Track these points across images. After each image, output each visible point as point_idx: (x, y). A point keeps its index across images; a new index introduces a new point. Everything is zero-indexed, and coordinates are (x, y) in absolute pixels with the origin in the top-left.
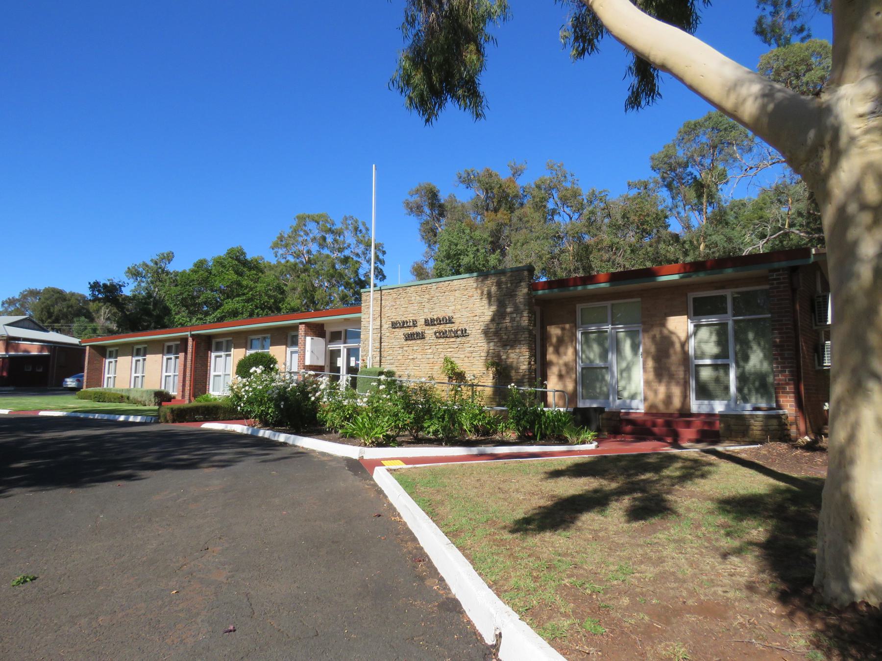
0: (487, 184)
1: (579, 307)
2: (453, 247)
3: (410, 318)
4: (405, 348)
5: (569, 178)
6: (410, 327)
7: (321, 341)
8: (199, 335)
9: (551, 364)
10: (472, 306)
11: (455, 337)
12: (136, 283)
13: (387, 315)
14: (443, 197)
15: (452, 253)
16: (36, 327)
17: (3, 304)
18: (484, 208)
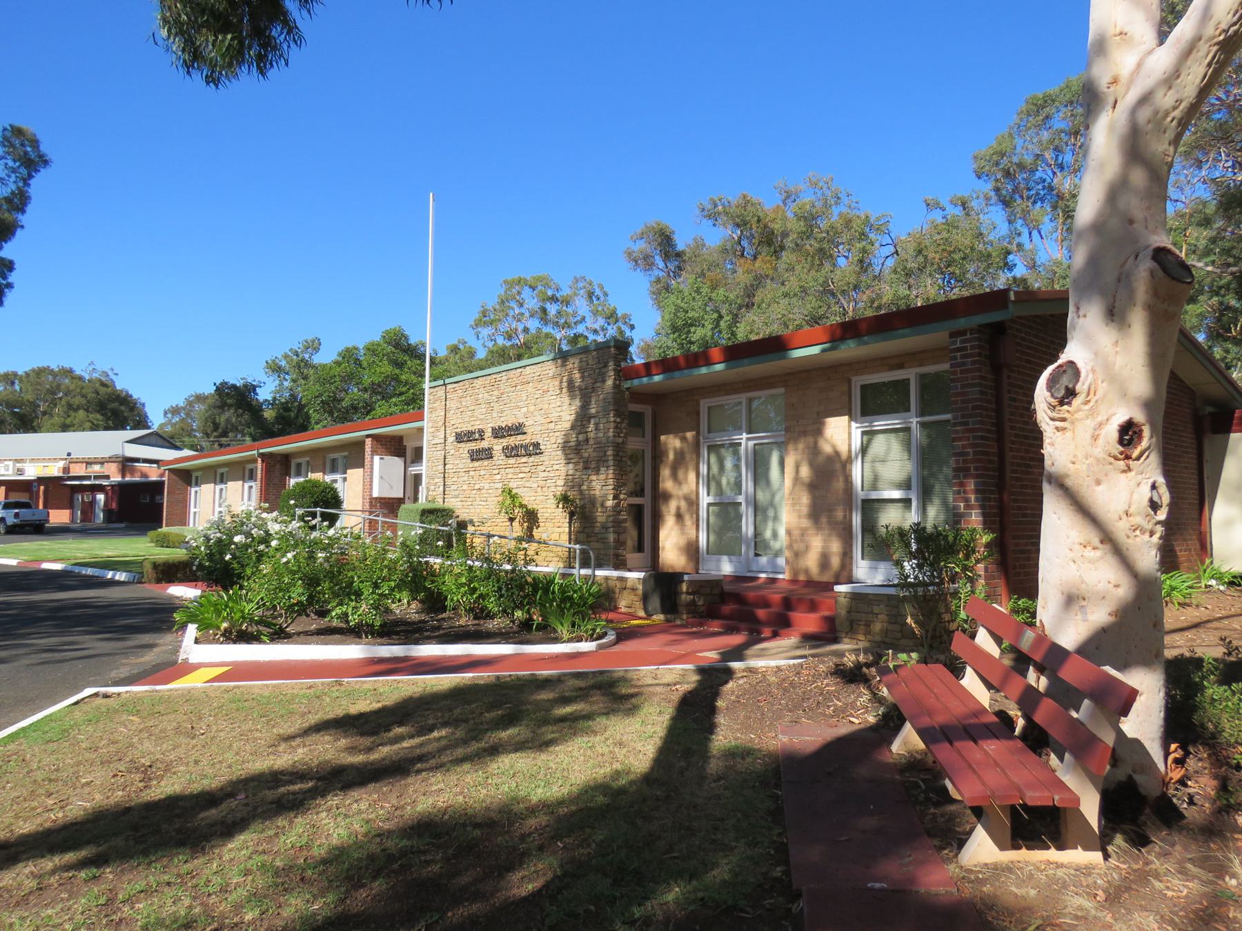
0: (738, 216)
1: (704, 404)
2: (681, 314)
3: (477, 426)
4: (472, 473)
5: (845, 200)
6: (476, 440)
7: (397, 462)
8: (271, 455)
9: (667, 497)
10: (546, 406)
11: (527, 455)
12: (277, 382)
13: (452, 422)
14: (682, 242)
15: (680, 323)
16: (166, 444)
17: (166, 413)
18: (735, 251)
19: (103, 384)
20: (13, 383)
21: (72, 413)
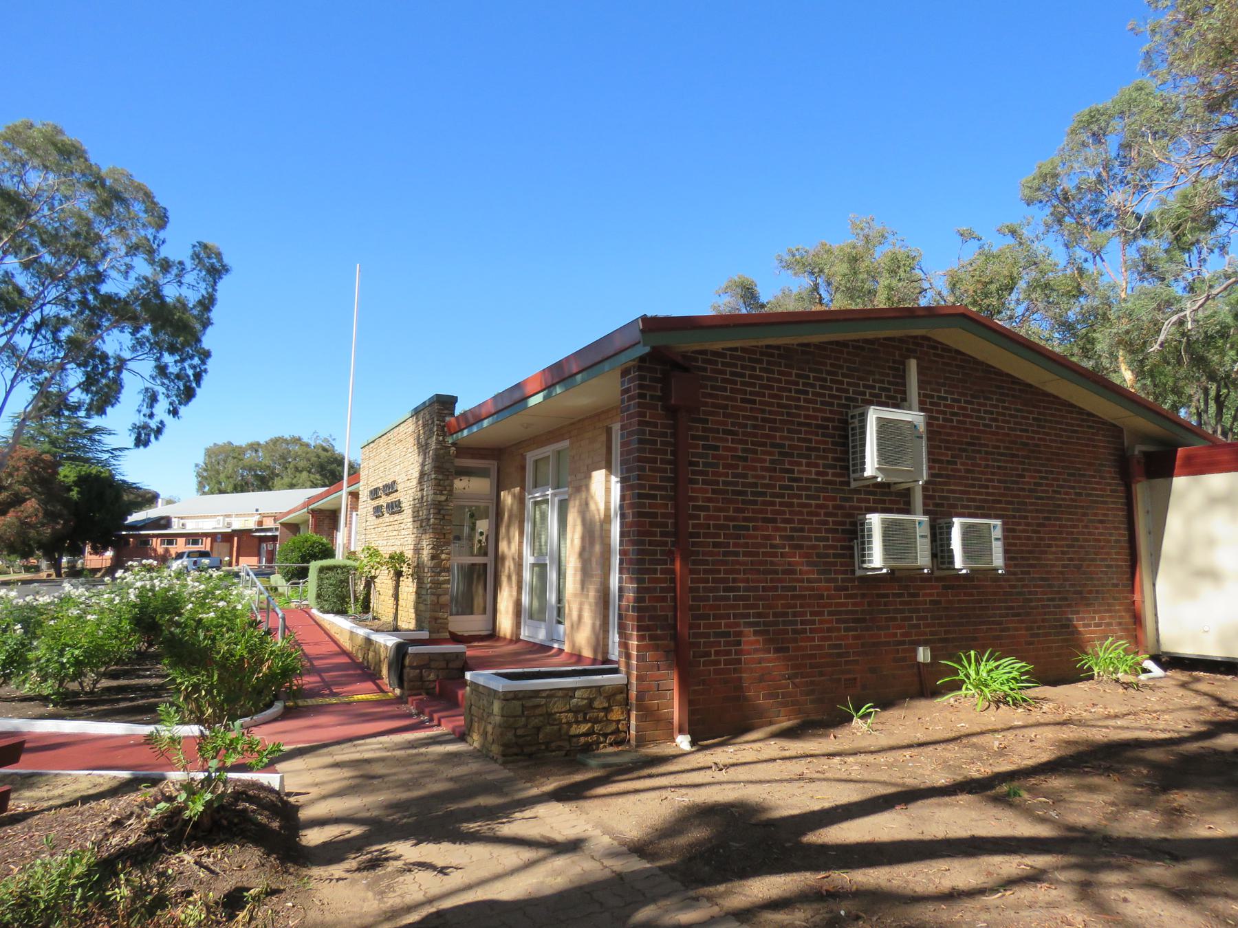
19: (325, 450)
20: (257, 451)
21: (298, 474)
